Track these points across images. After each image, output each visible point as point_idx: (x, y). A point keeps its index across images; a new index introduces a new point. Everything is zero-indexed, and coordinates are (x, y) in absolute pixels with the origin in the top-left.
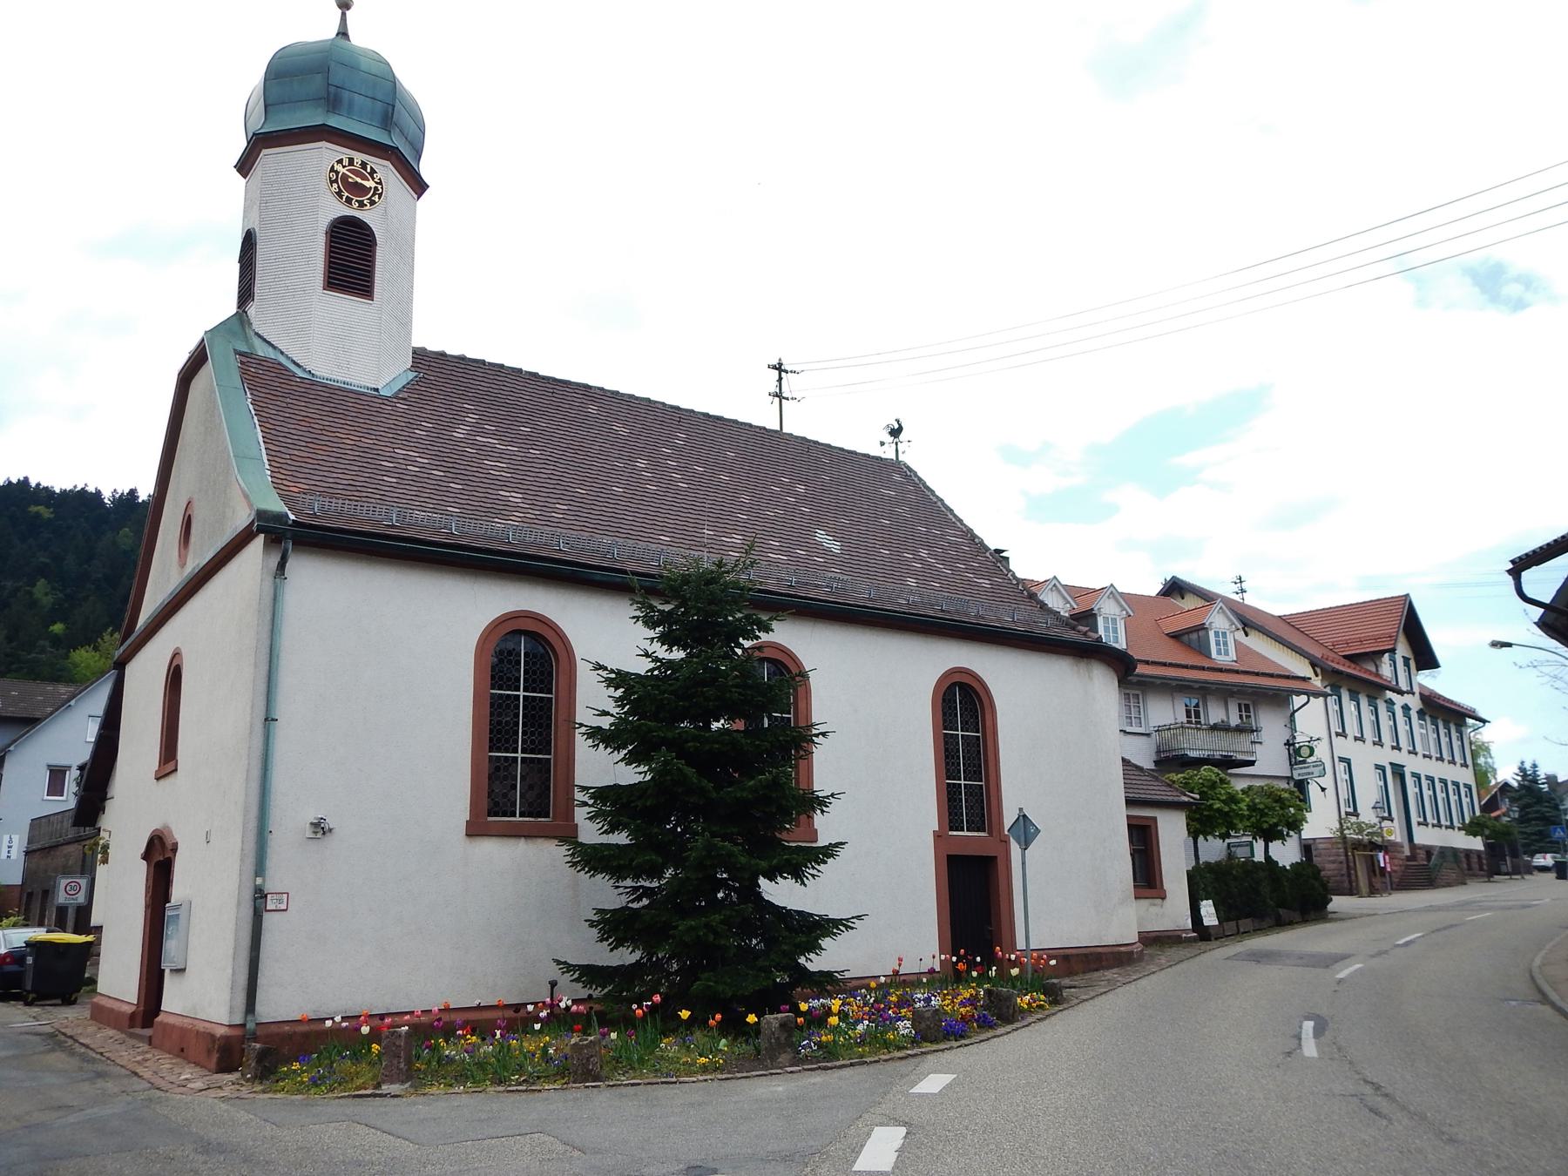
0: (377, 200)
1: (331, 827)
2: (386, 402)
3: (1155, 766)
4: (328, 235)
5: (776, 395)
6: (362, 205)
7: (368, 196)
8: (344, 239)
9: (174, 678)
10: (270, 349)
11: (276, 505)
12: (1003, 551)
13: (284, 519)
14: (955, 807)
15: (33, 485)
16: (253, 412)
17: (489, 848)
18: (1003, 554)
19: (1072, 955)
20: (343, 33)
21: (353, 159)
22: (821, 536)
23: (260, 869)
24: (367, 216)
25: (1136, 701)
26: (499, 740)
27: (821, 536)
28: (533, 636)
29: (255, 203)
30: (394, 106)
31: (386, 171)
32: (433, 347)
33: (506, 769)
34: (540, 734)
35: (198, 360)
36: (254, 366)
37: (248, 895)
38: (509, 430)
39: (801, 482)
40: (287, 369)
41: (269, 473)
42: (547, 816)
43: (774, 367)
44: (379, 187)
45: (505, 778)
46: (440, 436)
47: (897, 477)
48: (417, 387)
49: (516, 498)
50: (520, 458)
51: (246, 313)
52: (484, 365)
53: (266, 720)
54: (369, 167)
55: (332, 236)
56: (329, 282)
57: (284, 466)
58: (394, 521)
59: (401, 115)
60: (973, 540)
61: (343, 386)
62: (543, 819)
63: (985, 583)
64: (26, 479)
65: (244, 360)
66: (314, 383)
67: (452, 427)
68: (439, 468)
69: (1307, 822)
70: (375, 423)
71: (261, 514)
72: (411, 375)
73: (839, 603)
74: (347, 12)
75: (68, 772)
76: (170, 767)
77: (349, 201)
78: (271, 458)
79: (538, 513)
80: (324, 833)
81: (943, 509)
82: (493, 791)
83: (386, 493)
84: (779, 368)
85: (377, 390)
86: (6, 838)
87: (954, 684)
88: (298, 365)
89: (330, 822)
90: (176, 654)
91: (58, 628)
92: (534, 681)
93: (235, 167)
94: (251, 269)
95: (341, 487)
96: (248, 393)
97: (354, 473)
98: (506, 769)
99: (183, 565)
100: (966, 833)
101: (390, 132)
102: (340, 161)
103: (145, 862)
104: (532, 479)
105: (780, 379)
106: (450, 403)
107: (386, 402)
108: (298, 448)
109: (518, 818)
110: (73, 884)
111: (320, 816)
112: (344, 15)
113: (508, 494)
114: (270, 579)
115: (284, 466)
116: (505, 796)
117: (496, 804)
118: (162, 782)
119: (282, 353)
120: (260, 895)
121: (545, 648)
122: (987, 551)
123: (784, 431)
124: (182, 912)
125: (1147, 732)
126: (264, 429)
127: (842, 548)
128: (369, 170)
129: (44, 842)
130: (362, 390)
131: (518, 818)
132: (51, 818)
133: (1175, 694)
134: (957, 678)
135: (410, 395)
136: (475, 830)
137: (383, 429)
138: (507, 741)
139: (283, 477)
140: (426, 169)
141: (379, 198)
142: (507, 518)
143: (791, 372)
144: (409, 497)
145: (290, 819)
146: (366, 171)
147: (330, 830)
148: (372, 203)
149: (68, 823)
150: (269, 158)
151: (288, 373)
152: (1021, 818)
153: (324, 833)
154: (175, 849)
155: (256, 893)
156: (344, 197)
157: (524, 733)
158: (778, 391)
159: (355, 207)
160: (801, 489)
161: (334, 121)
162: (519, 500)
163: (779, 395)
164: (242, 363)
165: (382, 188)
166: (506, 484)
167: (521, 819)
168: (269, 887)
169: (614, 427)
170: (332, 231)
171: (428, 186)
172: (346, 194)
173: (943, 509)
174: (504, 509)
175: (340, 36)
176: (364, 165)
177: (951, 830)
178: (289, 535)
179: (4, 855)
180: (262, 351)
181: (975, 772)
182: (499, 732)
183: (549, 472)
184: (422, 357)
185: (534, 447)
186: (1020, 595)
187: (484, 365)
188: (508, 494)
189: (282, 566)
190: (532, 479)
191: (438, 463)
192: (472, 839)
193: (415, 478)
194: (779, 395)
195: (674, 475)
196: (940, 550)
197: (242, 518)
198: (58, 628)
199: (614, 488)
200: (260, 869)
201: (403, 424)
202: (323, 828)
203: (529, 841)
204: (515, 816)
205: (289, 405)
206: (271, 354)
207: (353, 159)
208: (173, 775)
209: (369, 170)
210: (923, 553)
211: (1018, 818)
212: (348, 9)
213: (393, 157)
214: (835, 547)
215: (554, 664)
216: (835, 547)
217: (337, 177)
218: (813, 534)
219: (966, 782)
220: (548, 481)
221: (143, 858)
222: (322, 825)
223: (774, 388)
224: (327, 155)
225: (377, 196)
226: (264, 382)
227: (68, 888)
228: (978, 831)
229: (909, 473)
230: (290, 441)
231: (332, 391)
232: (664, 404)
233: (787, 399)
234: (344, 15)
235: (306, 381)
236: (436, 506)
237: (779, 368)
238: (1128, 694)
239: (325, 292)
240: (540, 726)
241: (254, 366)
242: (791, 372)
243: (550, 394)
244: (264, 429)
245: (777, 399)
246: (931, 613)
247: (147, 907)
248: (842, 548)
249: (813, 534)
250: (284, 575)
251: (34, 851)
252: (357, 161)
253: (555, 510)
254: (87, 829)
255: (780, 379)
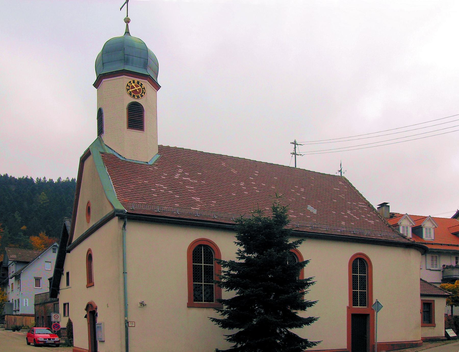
0: (143, 95)
1: (146, 304)
2: (151, 167)
3: (442, 281)
4: (128, 109)
5: (293, 154)
6: (138, 97)
7: (140, 94)
8: (133, 110)
9: (90, 257)
10: (111, 150)
11: (120, 207)
12: (388, 203)
13: (124, 212)
14: (356, 299)
15: (9, 176)
16: (108, 174)
17: (195, 312)
18: (387, 205)
19: (394, 344)
20: (127, 32)
21: (134, 81)
22: (310, 208)
23: (126, 315)
24: (140, 101)
25: (436, 259)
26: (196, 279)
27: (310, 208)
28: (206, 246)
29: (100, 98)
30: (147, 60)
31: (146, 84)
32: (165, 144)
33: (199, 287)
34: (210, 277)
35: (87, 154)
36: (106, 157)
37: (123, 322)
38: (194, 174)
39: (302, 187)
40: (117, 157)
41: (116, 195)
42: (213, 301)
43: (293, 143)
44: (144, 90)
45: (199, 290)
46: (170, 178)
47: (341, 183)
48: (161, 160)
49: (198, 199)
50: (198, 185)
51: (101, 137)
52: (183, 150)
53: (124, 273)
54: (140, 83)
55: (129, 109)
56: (129, 126)
57: (121, 193)
58: (158, 210)
59: (151, 63)
60: (369, 206)
61: (136, 162)
62: (212, 303)
63: (372, 222)
64: (7, 174)
65: (103, 155)
66: (126, 162)
67: (174, 174)
68: (171, 190)
69: (307, 339)
70: (148, 175)
71: (116, 211)
72: (158, 156)
73: (315, 233)
74: (129, 24)
75: (41, 280)
76: (91, 284)
77: (134, 96)
78: (116, 190)
79: (206, 204)
80: (144, 306)
81: (358, 195)
82: (195, 294)
83: (154, 200)
84: (295, 143)
85: (147, 162)
86: (24, 300)
87: (357, 259)
88: (120, 156)
89: (145, 303)
90: (89, 250)
91: (24, 228)
92: (207, 260)
93: (93, 85)
94: (102, 126)
95: (139, 199)
96: (106, 168)
97: (143, 194)
98: (199, 287)
99: (88, 221)
100: (359, 307)
101: (146, 69)
102: (130, 82)
103: (86, 311)
104: (203, 192)
105: (295, 148)
106: (173, 165)
107: (151, 167)
108: (124, 186)
109: (203, 302)
110: (56, 316)
111: (142, 301)
112: (127, 25)
113: (195, 198)
114: (121, 230)
115: (121, 193)
116: (199, 295)
117: (196, 298)
118: (89, 288)
119: (115, 151)
120: (127, 322)
121: (210, 250)
122: (374, 210)
123: (297, 167)
124: (102, 325)
125: (439, 269)
126: (113, 180)
127: (318, 212)
128: (140, 84)
129: (40, 301)
130: (142, 163)
131: (203, 302)
132: (42, 294)
133: (452, 256)
134: (358, 256)
135: (158, 163)
136: (190, 305)
137: (150, 177)
138: (199, 279)
139: (121, 196)
140: (160, 81)
141: (144, 94)
142: (195, 207)
143: (300, 145)
144: (162, 201)
145: (134, 301)
146: (139, 85)
147: (146, 305)
148: (142, 96)
149: (49, 295)
150: (106, 82)
151: (117, 159)
152: (377, 302)
153: (144, 306)
154: (96, 308)
155: (125, 321)
156: (132, 95)
157: (204, 277)
158: (294, 152)
159: (136, 98)
160: (302, 190)
161: (127, 68)
162: (199, 200)
163: (295, 154)
164: (102, 156)
165: (145, 90)
166: (194, 194)
167: (205, 302)
168: (129, 320)
169: (231, 171)
170: (129, 108)
171: (161, 87)
172: (133, 94)
173: (358, 195)
174: (195, 204)
175: (127, 33)
176: (138, 82)
177: (354, 306)
178: (126, 217)
179: (25, 305)
180: (108, 151)
181: (363, 286)
182: (196, 276)
183: (209, 189)
184: (162, 149)
185: (203, 180)
186: (386, 226)
187: (183, 150)
188: (195, 198)
189: (124, 226)
190: (203, 192)
191: (170, 188)
192: (189, 308)
193: (163, 194)
194: (295, 154)
195: (254, 187)
196: (355, 211)
197: (109, 210)
198: (24, 228)
199: (232, 194)
200: (126, 315)
201: (157, 175)
202: (143, 304)
203: (207, 309)
204: (202, 301)
205: (119, 171)
206: (111, 152)
207: (134, 81)
208: (93, 287)
209: (140, 84)
210: (349, 212)
211: (376, 303)
212: (129, 23)
213: (148, 79)
214: (315, 212)
215: (213, 255)
216: (315, 212)
217: (129, 88)
218: (306, 207)
219: (360, 291)
220: (209, 192)
221: (85, 310)
222: (143, 303)
223: (293, 151)
224: (125, 80)
225: (143, 93)
226: (110, 163)
227: (55, 316)
228: (364, 306)
229: (346, 181)
230: (121, 183)
231: (132, 164)
232: (250, 160)
233: (298, 155)
234: (127, 25)
235: (124, 161)
236: (171, 204)
237: (295, 143)
238: (433, 256)
239: (128, 129)
240: (210, 274)
241: (106, 157)
242: (300, 145)
243: (208, 159)
244: (113, 180)
245: (294, 155)
246: (350, 235)
247: (88, 324)
248: (318, 212)
249: (306, 207)
250: (125, 229)
251: (37, 304)
252: (136, 81)
253: (212, 203)
254: (54, 298)
255: (295, 148)
